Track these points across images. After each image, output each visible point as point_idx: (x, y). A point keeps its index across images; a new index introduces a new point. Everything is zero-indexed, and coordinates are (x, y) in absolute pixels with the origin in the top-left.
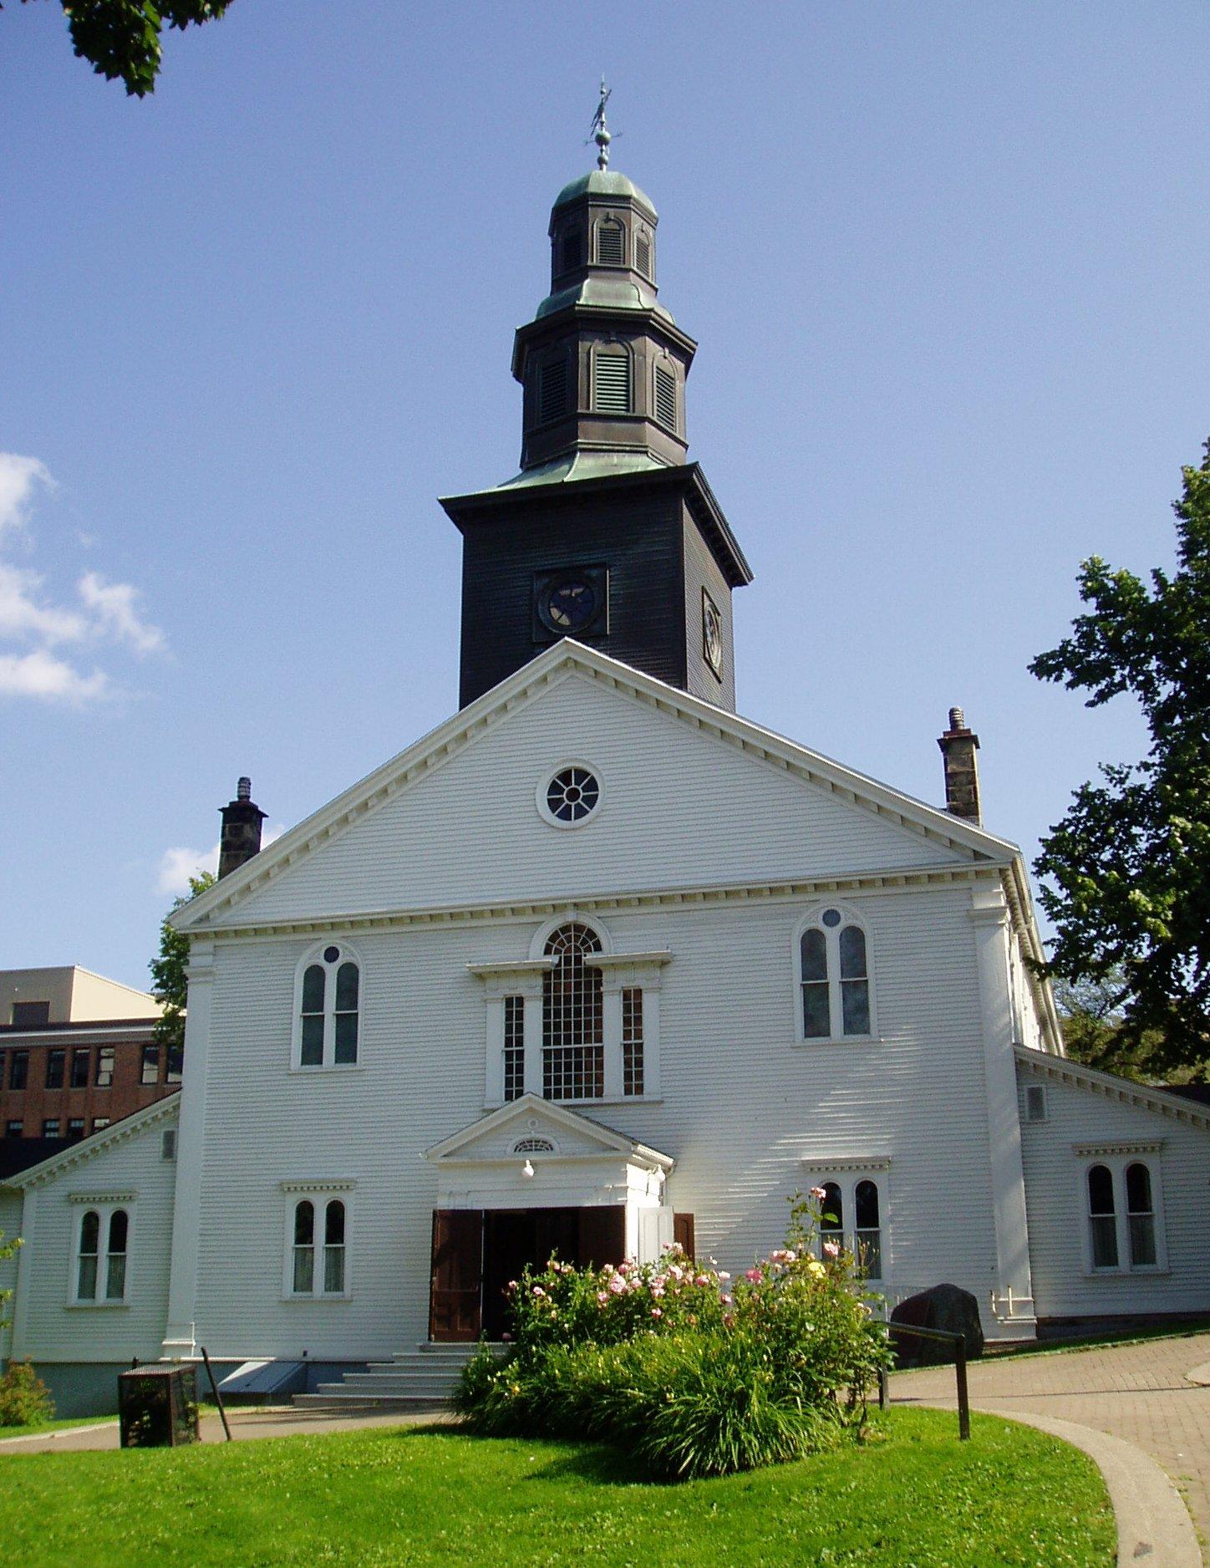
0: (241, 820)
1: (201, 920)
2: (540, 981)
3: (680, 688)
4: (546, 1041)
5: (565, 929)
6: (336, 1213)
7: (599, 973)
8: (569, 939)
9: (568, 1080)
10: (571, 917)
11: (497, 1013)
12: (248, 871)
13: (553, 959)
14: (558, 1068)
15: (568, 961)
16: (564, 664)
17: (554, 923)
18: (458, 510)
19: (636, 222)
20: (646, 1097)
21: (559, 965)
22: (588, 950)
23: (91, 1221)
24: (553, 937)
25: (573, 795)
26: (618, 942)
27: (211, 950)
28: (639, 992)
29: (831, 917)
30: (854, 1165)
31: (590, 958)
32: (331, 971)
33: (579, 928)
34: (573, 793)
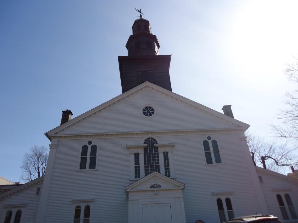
0: (66, 114)
1: (56, 133)
2: (143, 150)
3: (231, 210)
4: (145, 164)
5: (149, 139)
7: (157, 148)
8: (149, 141)
9: (150, 160)
10: (150, 136)
11: (132, 157)
12: (66, 125)
13: (146, 145)
14: (148, 157)
15: (149, 145)
17: (146, 137)
18: (62, 111)
22: (154, 143)
23: (10, 213)
24: (146, 140)
25: (149, 112)
26: (161, 141)
27: (57, 141)
28: (167, 153)
29: (90, 143)
31: (156, 145)
32: (89, 147)
33: (152, 139)
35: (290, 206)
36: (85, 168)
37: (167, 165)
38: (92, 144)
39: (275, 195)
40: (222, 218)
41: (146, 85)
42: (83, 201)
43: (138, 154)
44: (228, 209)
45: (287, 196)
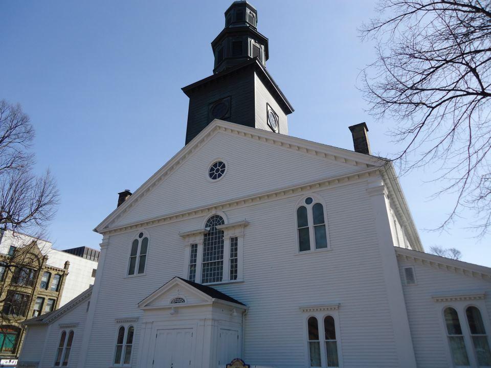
1: (106, 228)
2: (202, 237)
5: (212, 218)
6: (329, 322)
7: (223, 232)
10: (213, 212)
11: (188, 251)
13: (208, 229)
16: (42, 320)
19: (248, 11)
20: (237, 280)
21: (210, 231)
22: (216, 225)
24: (209, 221)
26: (231, 217)
27: (108, 237)
29: (309, 201)
30: (315, 309)
32: (309, 208)
34: (217, 170)
35: (452, 335)
36: (308, 248)
37: (235, 259)
38: (314, 203)
39: (440, 308)
40: (315, 357)
41: (215, 125)
42: (315, 309)
43: (196, 245)
44: (327, 338)
45: (472, 312)
